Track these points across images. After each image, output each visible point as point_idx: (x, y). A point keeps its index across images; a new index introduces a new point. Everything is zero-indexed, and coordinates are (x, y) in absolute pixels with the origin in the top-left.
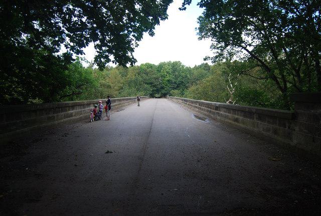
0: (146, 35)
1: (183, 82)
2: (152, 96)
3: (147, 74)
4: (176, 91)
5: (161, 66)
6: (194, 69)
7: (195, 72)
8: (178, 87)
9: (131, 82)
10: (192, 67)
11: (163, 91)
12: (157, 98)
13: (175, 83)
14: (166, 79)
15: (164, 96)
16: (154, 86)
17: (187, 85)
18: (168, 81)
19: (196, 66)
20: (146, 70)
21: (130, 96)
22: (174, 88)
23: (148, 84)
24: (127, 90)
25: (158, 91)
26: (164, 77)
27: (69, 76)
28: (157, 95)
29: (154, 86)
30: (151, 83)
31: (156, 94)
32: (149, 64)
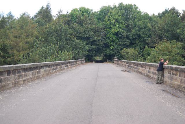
0: (45, 7)
1: (139, 36)
2: (90, 59)
3: (81, 23)
4: (131, 51)
5: (105, 12)
6: (157, 17)
7: (161, 22)
8: (132, 44)
9: (50, 34)
10: (156, 14)
11: (108, 52)
12: (97, 62)
13: (127, 37)
14: (114, 31)
15: (108, 58)
16: (93, 43)
17: (149, 40)
18: (117, 34)
19: (45, 13)
20: (79, 17)
21: (45, 59)
22: (127, 46)
23: (83, 39)
24: (43, 49)
25: (99, 51)
26: (110, 28)
27: (145, 13)
28: (98, 58)
29: (93, 43)
30: (88, 38)
31: (96, 55)
32: (84, 9)
